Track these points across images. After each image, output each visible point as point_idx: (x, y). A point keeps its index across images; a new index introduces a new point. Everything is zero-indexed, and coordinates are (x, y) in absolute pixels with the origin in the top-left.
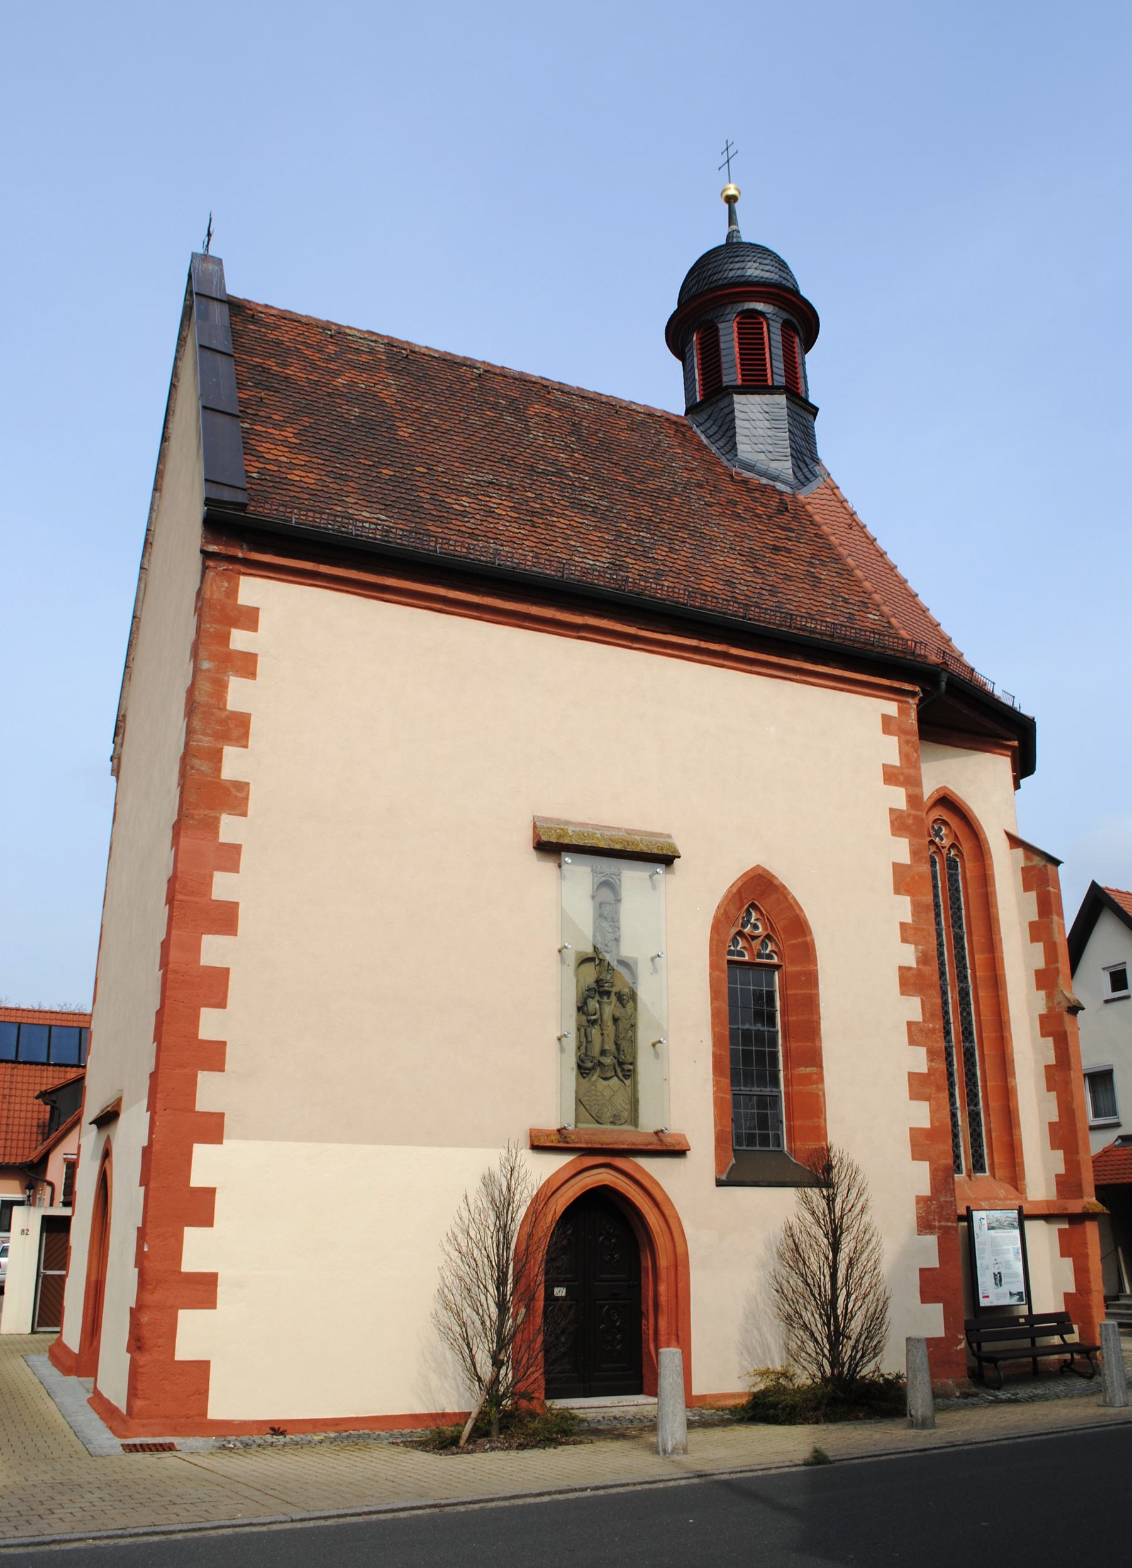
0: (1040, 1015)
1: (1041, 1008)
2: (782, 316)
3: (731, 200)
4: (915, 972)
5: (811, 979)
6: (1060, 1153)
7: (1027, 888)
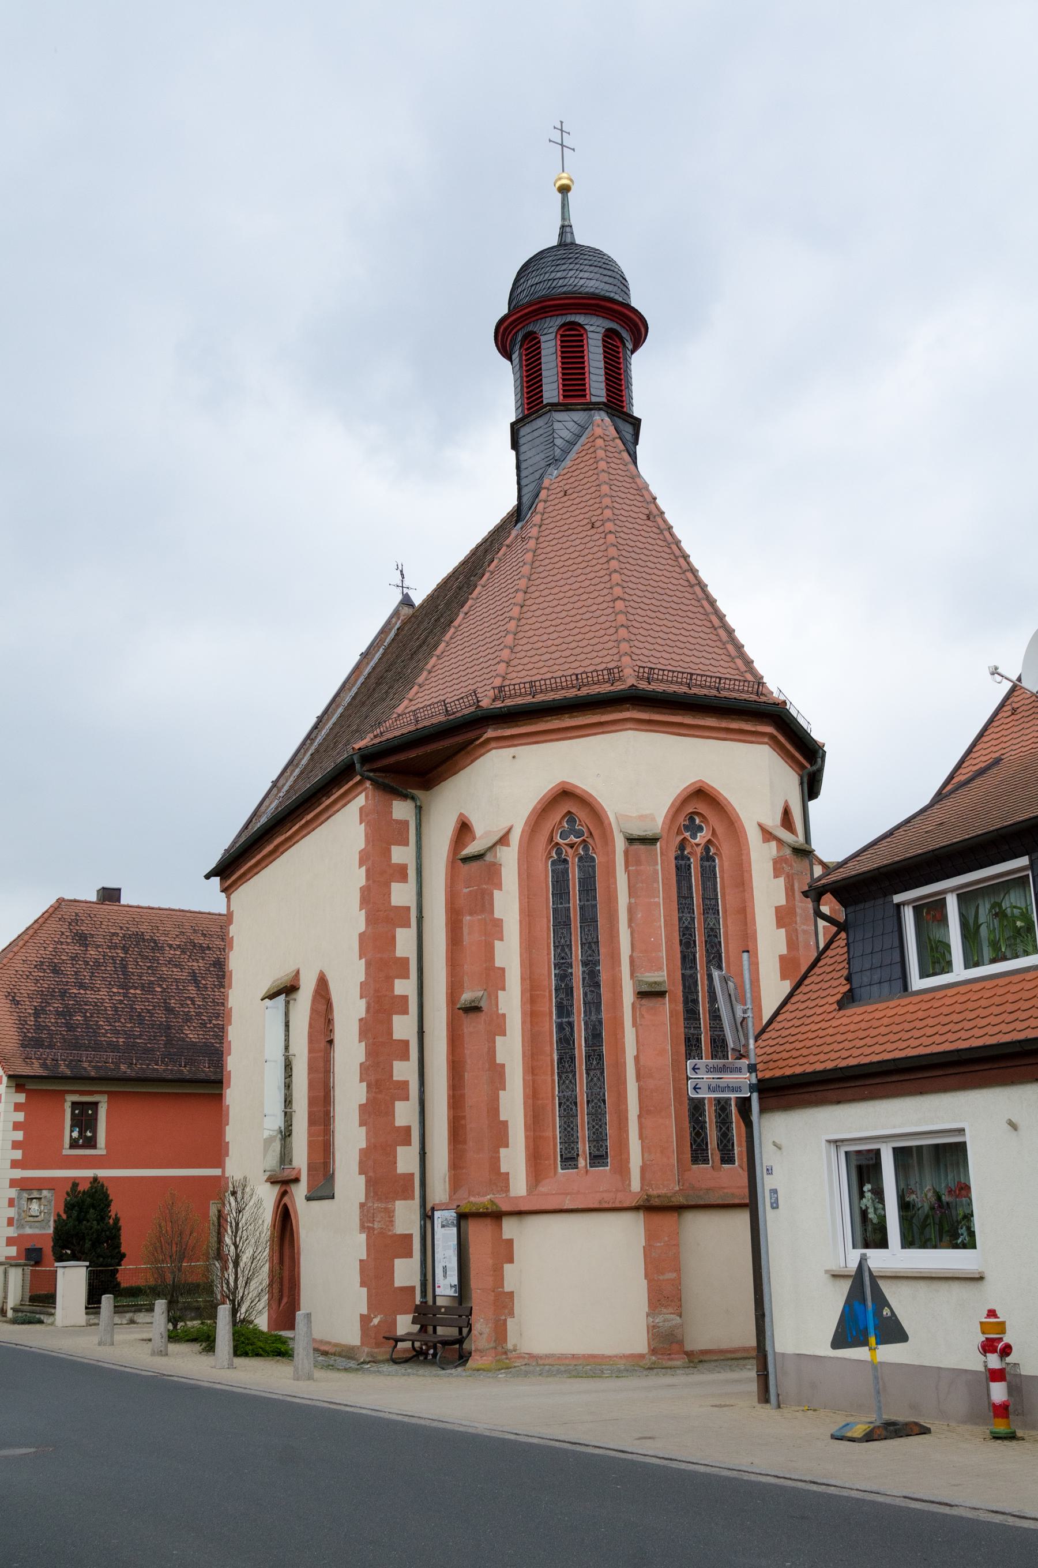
2: (604, 325)
3: (564, 190)
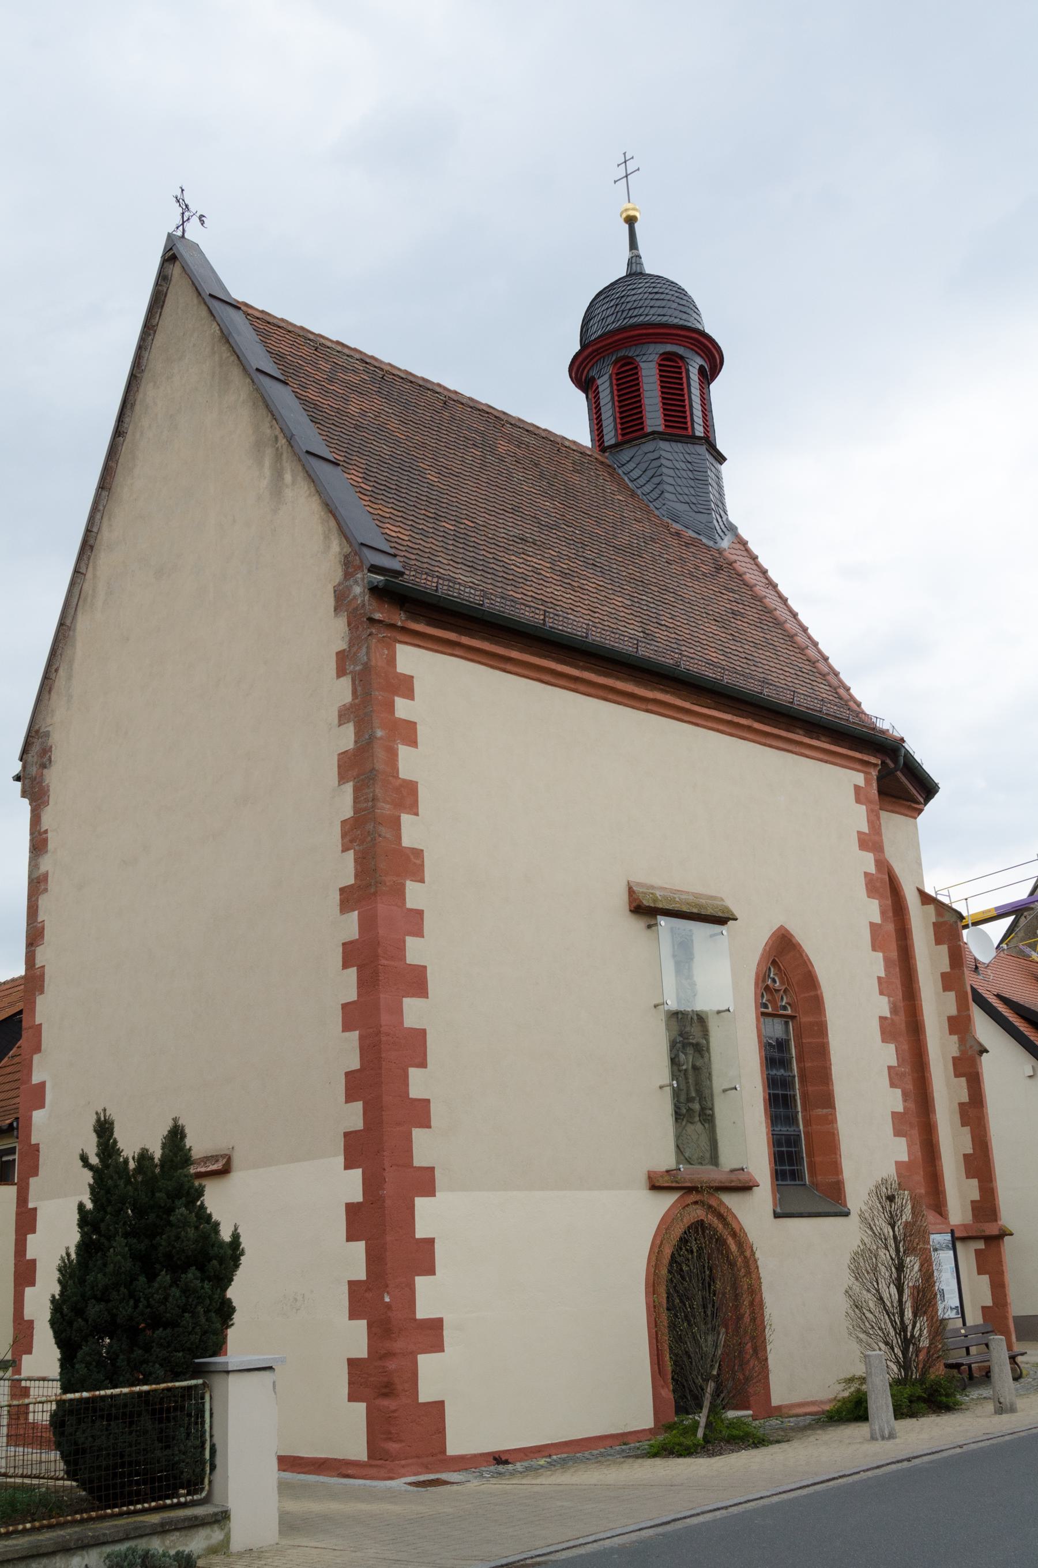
0: (953, 1057)
1: (954, 1050)
3: (631, 221)
4: (890, 1021)
5: (821, 1029)
6: (975, 1182)
7: (938, 941)
